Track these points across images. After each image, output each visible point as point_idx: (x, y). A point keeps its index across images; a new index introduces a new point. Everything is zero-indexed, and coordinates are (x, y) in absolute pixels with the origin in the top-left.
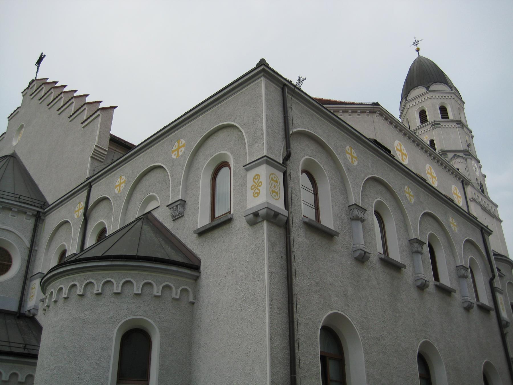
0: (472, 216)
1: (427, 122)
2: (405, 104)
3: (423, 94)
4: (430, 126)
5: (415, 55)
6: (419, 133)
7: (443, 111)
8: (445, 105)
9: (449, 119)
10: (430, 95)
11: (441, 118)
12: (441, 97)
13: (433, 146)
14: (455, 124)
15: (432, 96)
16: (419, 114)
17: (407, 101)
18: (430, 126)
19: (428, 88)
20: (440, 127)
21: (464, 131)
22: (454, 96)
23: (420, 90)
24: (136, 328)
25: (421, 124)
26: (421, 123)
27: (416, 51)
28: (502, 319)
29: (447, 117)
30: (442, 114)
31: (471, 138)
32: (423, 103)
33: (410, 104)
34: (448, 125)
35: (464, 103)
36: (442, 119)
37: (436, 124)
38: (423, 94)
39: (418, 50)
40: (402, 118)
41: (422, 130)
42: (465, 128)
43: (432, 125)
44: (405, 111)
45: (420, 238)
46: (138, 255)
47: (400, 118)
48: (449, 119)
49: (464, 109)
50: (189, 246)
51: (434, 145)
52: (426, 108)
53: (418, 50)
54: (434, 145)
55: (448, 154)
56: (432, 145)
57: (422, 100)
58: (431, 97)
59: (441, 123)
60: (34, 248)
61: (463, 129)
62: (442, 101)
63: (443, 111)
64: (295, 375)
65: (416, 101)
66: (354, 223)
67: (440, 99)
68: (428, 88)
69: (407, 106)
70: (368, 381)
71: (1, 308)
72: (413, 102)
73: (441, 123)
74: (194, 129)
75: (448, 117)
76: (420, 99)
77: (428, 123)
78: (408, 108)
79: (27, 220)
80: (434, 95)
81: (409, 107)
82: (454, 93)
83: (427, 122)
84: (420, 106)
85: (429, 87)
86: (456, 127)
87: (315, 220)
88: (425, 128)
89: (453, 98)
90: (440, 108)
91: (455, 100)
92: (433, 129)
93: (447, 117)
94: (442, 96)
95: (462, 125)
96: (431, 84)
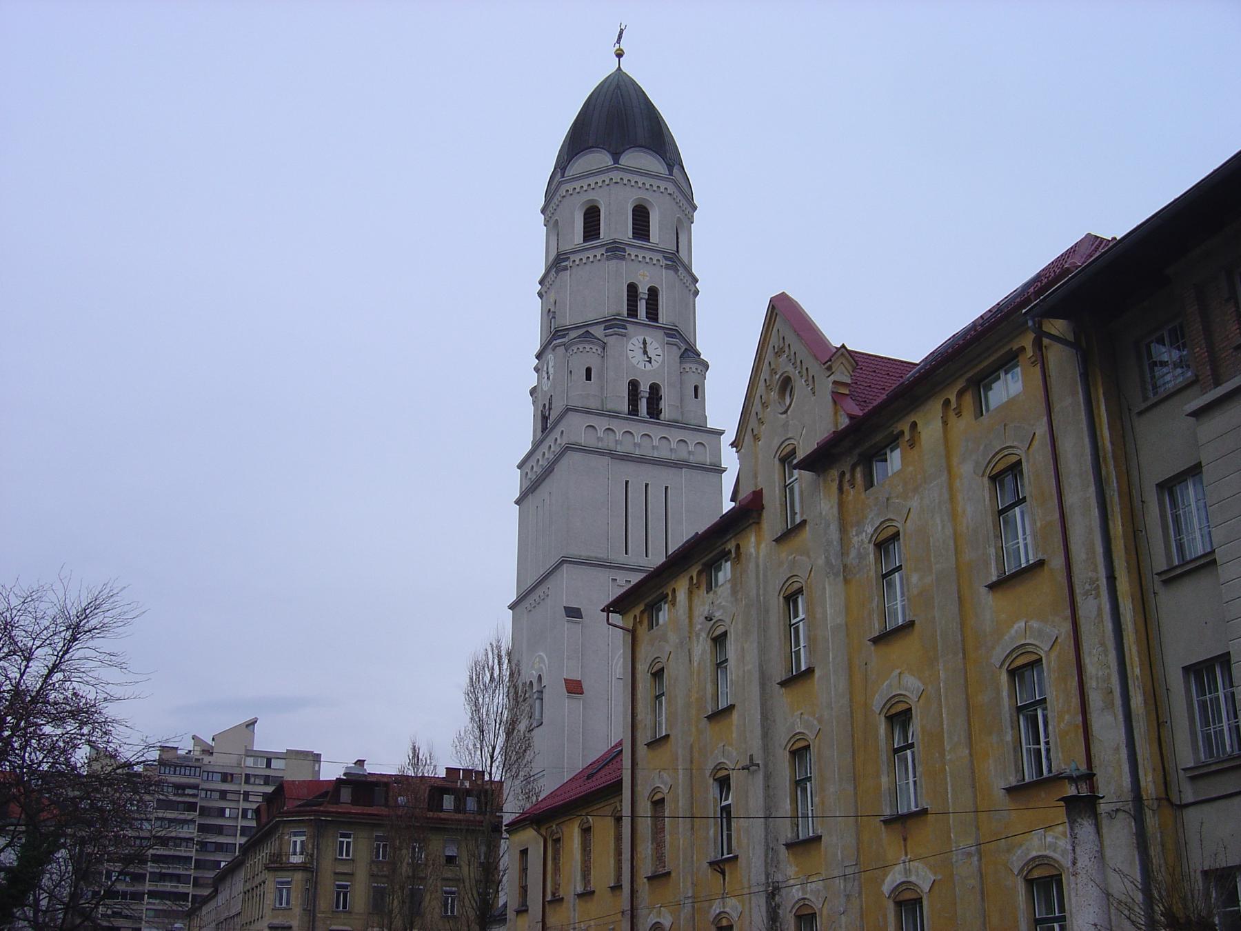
0: (1103, 473)
1: (599, 238)
2: (560, 183)
4: (603, 250)
5: (607, 68)
6: (574, 261)
7: (641, 216)
10: (616, 176)
11: (631, 237)
12: (648, 187)
14: (660, 257)
15: (622, 179)
16: (585, 214)
17: (563, 177)
18: (603, 250)
19: (616, 157)
20: (623, 258)
21: (678, 276)
22: (671, 189)
23: (601, 159)
25: (585, 241)
27: (615, 56)
29: (645, 235)
31: (692, 296)
33: (570, 187)
34: (636, 256)
35: (695, 208)
36: (634, 238)
37: (617, 249)
38: (608, 170)
39: (620, 55)
40: (547, 213)
41: (584, 255)
42: (681, 270)
44: (555, 201)
47: (542, 212)
49: (692, 223)
51: (596, 218)
52: (603, 206)
53: (620, 55)
54: (596, 218)
55: (628, 328)
57: (597, 183)
58: (619, 181)
59: (628, 250)
61: (676, 271)
62: (586, 197)
63: (641, 216)
64: (127, 892)
65: (584, 183)
67: (592, 191)
68: (616, 157)
69: (562, 191)
72: (577, 185)
73: (628, 250)
75: (649, 239)
76: (591, 181)
77: (649, 244)
78: (564, 197)
80: (627, 176)
81: (564, 194)
82: (676, 183)
83: (599, 238)
86: (662, 266)
87: (899, 450)
88: (591, 254)
89: (669, 192)
91: (674, 199)
92: (608, 259)
93: (645, 235)
96: (628, 149)
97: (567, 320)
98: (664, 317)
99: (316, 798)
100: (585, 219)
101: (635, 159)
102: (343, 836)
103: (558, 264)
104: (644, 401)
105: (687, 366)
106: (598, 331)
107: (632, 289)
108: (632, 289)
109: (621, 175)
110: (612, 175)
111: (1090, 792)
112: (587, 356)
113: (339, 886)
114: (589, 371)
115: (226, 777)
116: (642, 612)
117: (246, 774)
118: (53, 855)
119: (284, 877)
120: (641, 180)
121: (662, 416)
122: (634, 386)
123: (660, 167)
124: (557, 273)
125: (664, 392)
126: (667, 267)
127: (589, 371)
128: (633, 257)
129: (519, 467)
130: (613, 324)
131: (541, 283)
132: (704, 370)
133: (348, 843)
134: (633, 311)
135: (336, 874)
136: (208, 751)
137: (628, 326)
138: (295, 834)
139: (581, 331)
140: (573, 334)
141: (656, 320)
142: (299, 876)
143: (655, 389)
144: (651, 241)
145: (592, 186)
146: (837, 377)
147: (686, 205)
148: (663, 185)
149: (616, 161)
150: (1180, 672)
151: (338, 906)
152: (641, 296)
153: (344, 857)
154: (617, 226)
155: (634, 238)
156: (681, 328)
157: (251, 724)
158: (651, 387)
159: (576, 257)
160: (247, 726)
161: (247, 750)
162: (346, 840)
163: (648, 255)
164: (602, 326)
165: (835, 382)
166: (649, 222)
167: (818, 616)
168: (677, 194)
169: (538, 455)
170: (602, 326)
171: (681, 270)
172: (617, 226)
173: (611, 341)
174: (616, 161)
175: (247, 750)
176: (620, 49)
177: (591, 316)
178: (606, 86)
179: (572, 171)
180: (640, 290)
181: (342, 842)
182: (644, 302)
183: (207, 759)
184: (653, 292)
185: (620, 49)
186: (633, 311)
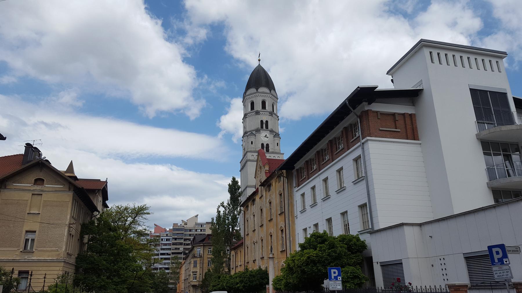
1: (254, 110)
7: (264, 103)
8: (265, 101)
10: (257, 94)
22: (271, 96)
23: (253, 90)
25: (251, 110)
28: (241, 167)
32: (267, 98)
33: (247, 97)
36: (262, 109)
38: (255, 93)
39: (259, 60)
41: (251, 114)
46: (374, 263)
50: (495, 259)
53: (259, 60)
60: (137, 280)
62: (251, 100)
63: (264, 103)
70: (517, 292)
72: (249, 97)
79: (42, 178)
80: (260, 94)
82: (272, 94)
83: (254, 110)
84: (252, 99)
85: (258, 89)
88: (252, 114)
92: (256, 115)
94: (268, 96)
97: (248, 130)
98: (270, 127)
99: (199, 242)
100: (251, 105)
101: (262, 89)
102: (209, 248)
103: (245, 116)
104: (265, 148)
105: (275, 138)
106: (254, 132)
107: (262, 121)
108: (262, 121)
109: (258, 94)
110: (256, 94)
111: (182, 254)
112: (252, 139)
113: (208, 261)
115: (190, 230)
116: (246, 207)
117: (196, 229)
118: (10, 291)
119: (195, 259)
120: (263, 95)
121: (269, 151)
122: (262, 145)
123: (268, 91)
124: (245, 118)
125: (270, 145)
126: (270, 115)
128: (262, 114)
129: (240, 163)
130: (258, 131)
131: (243, 120)
132: (279, 139)
133: (211, 250)
134: (262, 127)
135: (208, 258)
136: (186, 224)
137: (261, 131)
138: (198, 249)
139: (251, 132)
140: (249, 133)
141: (268, 128)
142: (199, 259)
143: (268, 145)
145: (252, 97)
146: (266, 169)
147: (275, 99)
148: (268, 95)
149: (257, 91)
150: (357, 209)
151: (208, 266)
152: (264, 123)
153: (210, 254)
154: (258, 107)
155: (262, 109)
156: (274, 130)
157: (196, 216)
158: (267, 144)
159: (249, 115)
160: (196, 217)
161: (196, 223)
162: (210, 249)
163: (265, 113)
164: (255, 131)
165: (265, 170)
166: (266, 106)
167: (187, 240)
168: (272, 97)
169: (244, 160)
170: (255, 131)
171: (274, 115)
172: (258, 107)
173: (257, 134)
174: (257, 91)
175: (196, 223)
176: (259, 59)
177: (253, 129)
178: (256, 70)
179: (247, 94)
180: (264, 122)
181: (209, 250)
182: (265, 124)
183: (185, 226)
184: (267, 122)
185: (259, 59)
186: (262, 127)
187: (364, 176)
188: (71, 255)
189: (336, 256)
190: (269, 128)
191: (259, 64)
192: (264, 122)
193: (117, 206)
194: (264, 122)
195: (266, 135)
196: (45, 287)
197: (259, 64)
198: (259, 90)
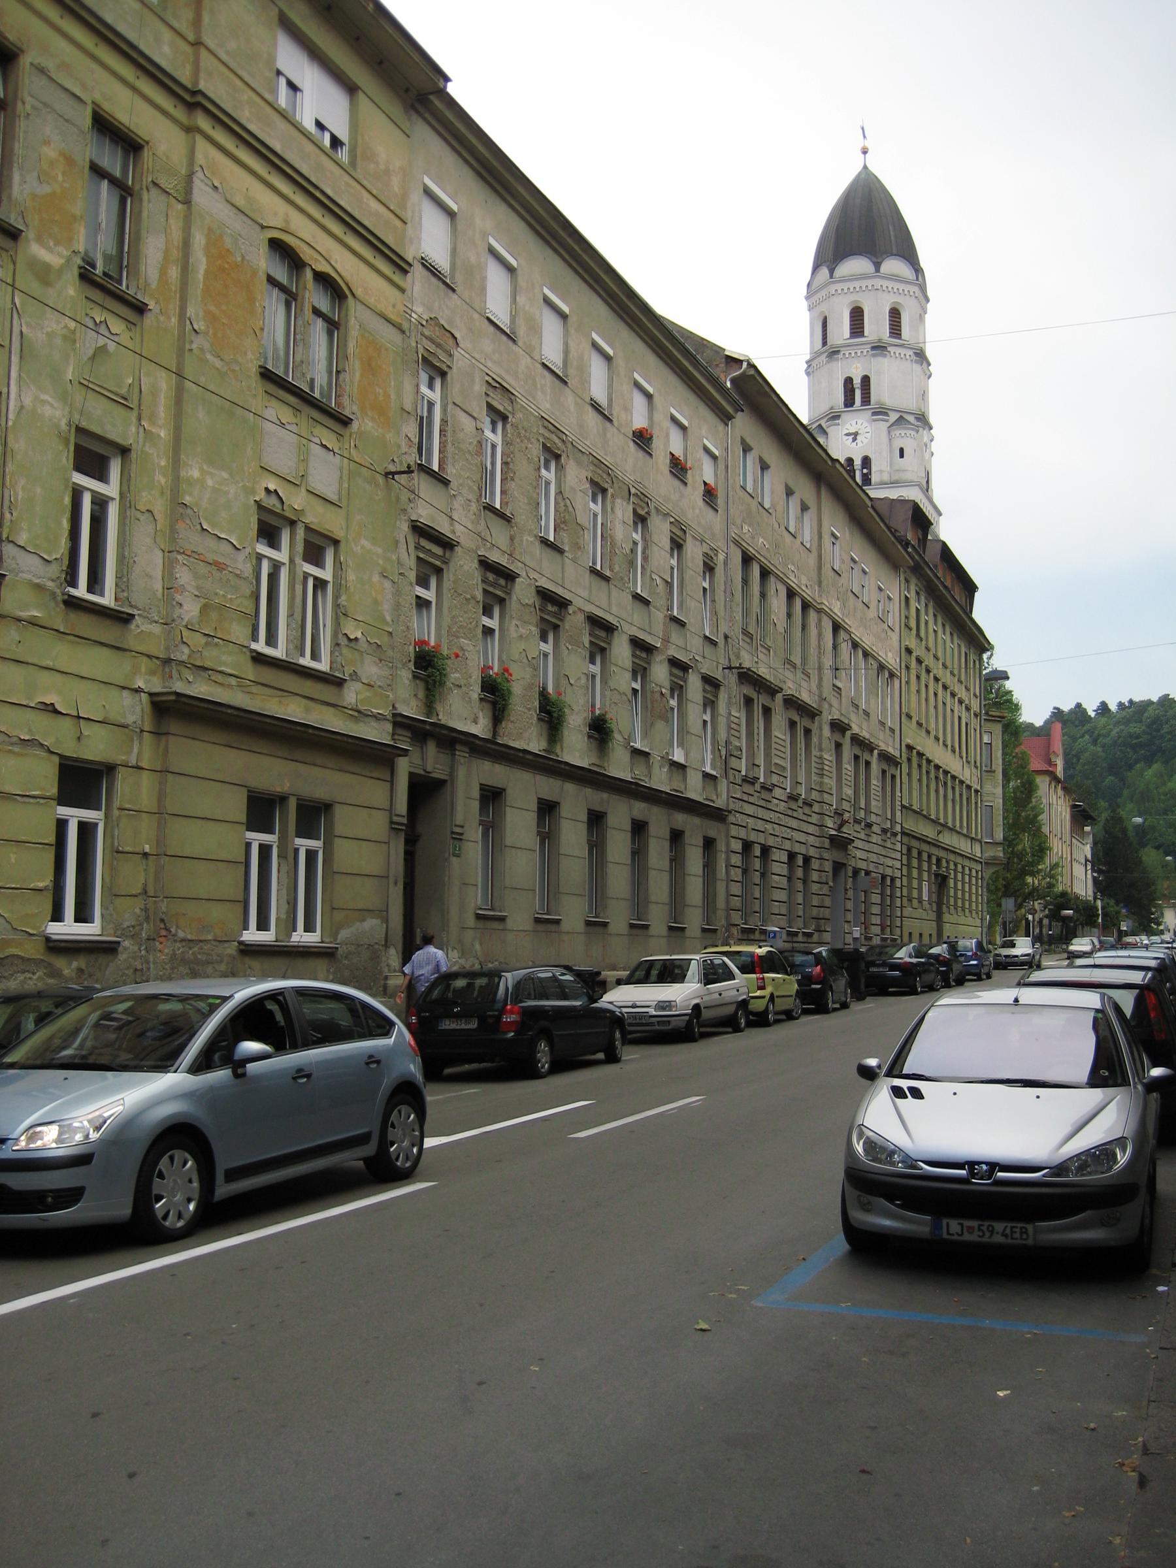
1: (870, 405)
3: (863, 277)
7: (857, 315)
9: (900, 338)
10: (832, 288)
13: (866, 384)
19: (877, 266)
23: (857, 265)
24: (190, 1122)
25: (862, 406)
26: (851, 333)
30: (893, 329)
38: (863, 277)
39: (865, 152)
42: (925, 363)
43: (873, 413)
45: (642, 971)
48: (900, 338)
51: (813, 299)
53: (865, 152)
56: (867, 393)
58: (879, 287)
66: (461, 824)
71: (3, 1157)
73: (889, 349)
74: (178, 653)
83: (494, 630)
90: (889, 312)
95: (920, 356)
101: (893, 265)
107: (849, 381)
114: (902, 456)
127: (902, 456)
144: (903, 337)
184: (866, 380)
186: (849, 402)
187: (758, 897)
188: (840, 416)
189: (1023, 811)
190: (873, 399)
191: (865, 167)
192: (857, 382)
193: (148, 906)
194: (857, 382)
195: (854, 439)
196: (733, 666)
197: (865, 167)
198: (837, 273)
